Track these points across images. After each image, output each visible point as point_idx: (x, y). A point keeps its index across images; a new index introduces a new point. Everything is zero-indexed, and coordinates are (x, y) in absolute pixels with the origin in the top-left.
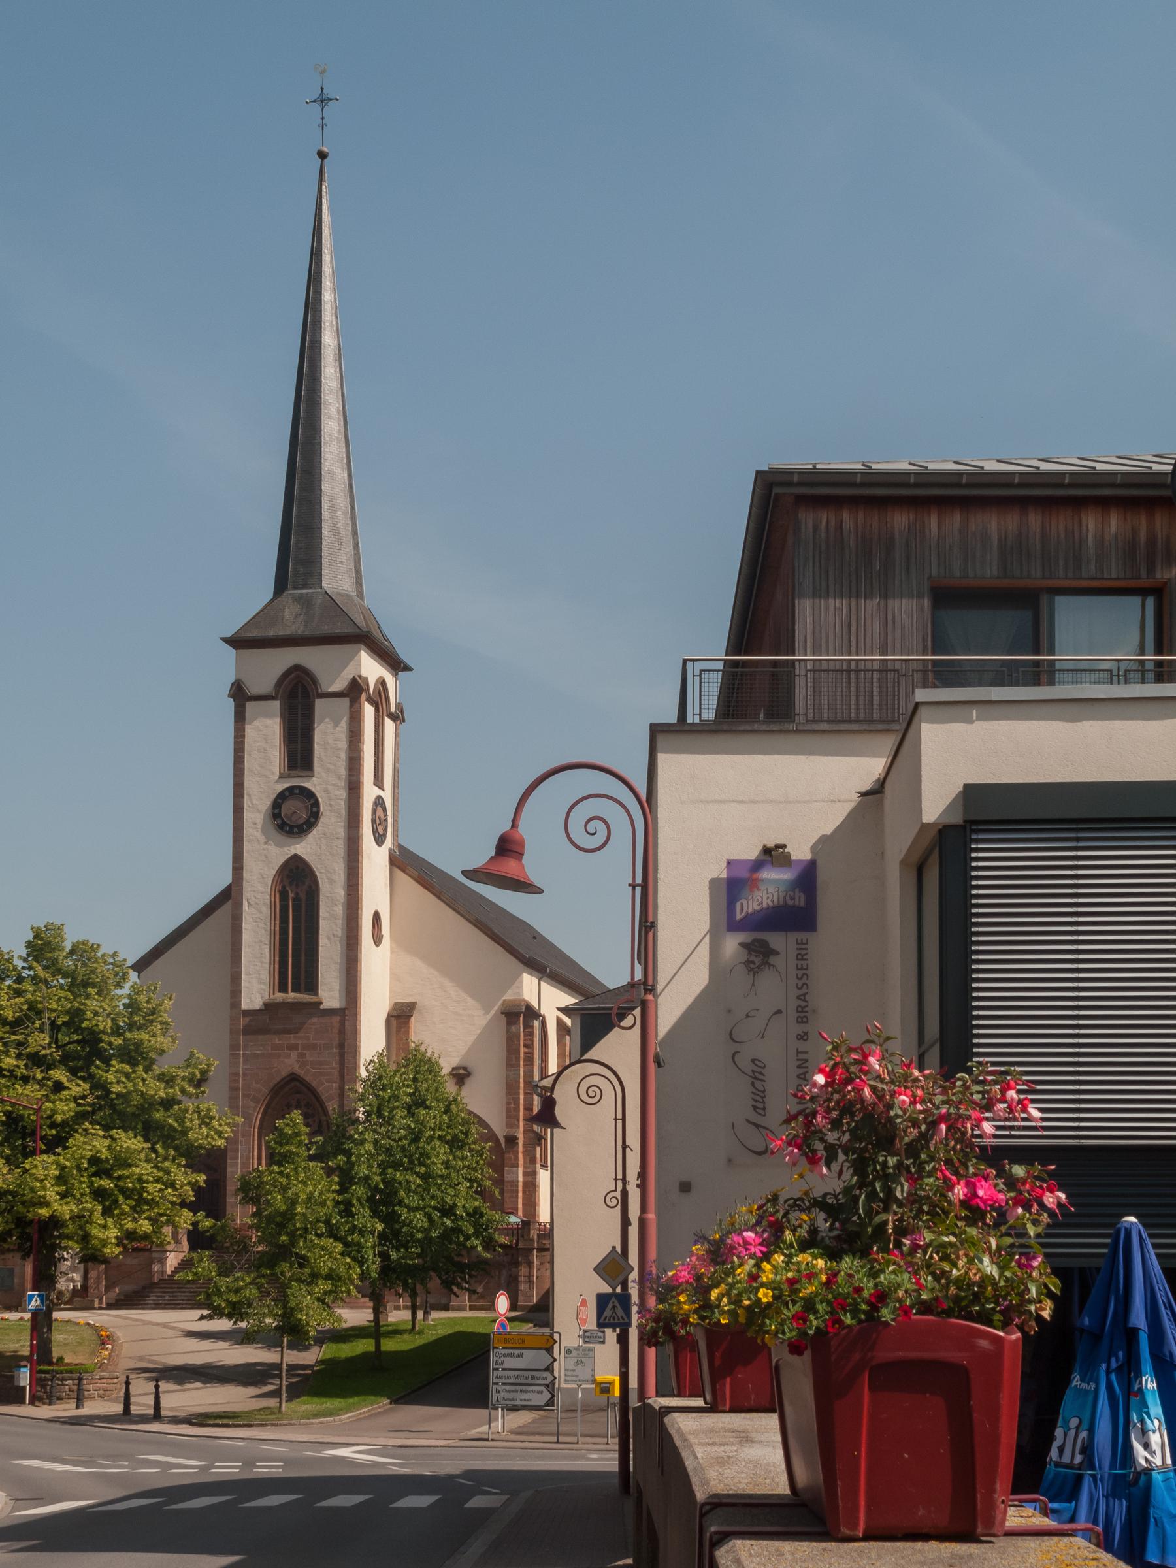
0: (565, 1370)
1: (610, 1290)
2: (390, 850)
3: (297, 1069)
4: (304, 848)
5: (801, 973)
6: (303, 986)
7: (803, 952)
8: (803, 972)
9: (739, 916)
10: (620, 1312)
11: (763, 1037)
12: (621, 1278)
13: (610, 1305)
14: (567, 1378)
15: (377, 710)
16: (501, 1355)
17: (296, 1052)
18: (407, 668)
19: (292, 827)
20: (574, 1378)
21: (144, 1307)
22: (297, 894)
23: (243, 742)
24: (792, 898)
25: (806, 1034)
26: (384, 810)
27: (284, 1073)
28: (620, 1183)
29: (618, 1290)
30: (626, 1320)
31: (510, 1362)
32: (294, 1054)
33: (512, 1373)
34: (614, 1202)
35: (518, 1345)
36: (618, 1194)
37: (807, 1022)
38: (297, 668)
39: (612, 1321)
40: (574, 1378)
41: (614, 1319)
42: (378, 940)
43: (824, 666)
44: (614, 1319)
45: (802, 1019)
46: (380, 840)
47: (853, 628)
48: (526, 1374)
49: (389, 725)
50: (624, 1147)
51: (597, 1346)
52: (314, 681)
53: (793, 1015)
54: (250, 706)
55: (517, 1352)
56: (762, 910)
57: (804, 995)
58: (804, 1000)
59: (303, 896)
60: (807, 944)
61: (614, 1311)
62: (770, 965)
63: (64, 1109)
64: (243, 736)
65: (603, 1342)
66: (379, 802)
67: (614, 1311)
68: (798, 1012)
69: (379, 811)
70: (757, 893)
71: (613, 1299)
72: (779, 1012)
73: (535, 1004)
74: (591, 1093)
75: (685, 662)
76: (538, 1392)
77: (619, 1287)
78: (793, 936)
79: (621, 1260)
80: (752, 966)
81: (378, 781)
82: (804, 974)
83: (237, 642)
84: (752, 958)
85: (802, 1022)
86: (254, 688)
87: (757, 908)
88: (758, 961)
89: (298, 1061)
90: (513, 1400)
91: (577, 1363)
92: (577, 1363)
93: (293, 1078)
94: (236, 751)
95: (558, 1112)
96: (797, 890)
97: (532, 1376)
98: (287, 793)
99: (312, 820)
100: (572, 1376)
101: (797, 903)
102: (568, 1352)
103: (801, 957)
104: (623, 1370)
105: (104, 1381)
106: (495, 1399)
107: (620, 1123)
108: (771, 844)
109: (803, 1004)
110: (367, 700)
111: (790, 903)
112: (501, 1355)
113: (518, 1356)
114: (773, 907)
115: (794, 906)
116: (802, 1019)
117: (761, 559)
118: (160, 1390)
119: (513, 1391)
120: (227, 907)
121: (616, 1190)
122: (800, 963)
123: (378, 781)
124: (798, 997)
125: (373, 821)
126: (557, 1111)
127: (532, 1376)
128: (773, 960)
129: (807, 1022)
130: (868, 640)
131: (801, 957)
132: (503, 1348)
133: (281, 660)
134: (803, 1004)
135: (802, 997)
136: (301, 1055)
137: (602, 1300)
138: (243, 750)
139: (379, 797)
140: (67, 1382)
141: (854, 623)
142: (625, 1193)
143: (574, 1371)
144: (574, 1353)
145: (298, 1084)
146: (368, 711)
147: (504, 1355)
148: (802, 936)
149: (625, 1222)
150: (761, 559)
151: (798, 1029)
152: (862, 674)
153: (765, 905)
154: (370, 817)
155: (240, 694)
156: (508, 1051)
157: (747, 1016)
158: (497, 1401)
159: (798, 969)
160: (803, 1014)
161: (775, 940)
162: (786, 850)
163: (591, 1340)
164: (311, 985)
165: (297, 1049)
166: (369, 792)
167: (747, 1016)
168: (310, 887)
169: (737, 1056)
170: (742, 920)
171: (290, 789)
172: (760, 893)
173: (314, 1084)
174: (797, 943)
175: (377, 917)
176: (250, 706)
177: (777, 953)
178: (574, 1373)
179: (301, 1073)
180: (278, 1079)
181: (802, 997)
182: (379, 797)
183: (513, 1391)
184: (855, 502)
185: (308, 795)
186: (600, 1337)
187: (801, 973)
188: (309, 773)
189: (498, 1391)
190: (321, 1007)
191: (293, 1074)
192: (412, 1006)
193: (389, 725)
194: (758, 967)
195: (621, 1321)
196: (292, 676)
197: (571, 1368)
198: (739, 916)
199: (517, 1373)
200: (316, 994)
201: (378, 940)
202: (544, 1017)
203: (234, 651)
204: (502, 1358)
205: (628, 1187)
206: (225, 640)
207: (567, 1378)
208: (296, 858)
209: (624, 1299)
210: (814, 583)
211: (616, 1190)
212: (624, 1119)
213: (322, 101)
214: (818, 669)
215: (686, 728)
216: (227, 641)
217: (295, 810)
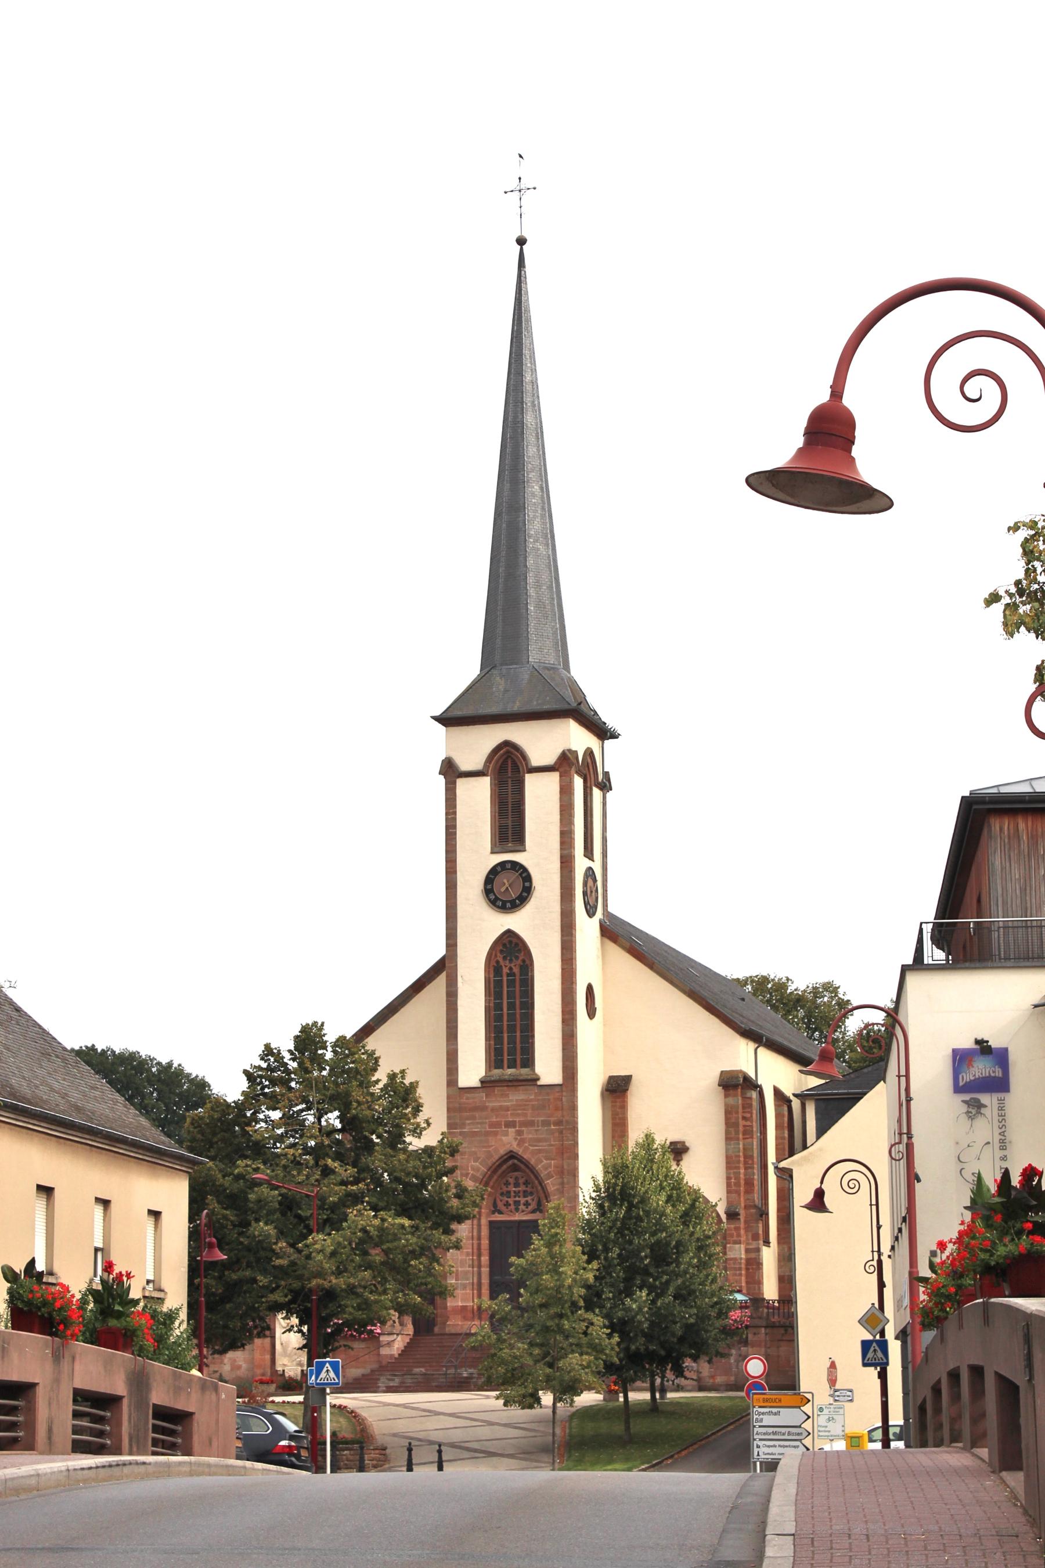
0: (818, 1426)
1: (871, 1338)
2: (600, 920)
3: (515, 1147)
4: (517, 922)
5: (1001, 1118)
6: (518, 1062)
7: (1002, 1105)
8: (1002, 1117)
9: (961, 1084)
10: (880, 1354)
11: (979, 1159)
12: (879, 1328)
13: (872, 1349)
14: (821, 1434)
15: (585, 782)
16: (760, 1414)
17: (513, 1130)
18: (614, 736)
19: (504, 903)
20: (827, 1434)
21: (375, 1390)
22: (511, 969)
23: (455, 819)
24: (994, 1072)
25: (1006, 1156)
26: (595, 880)
27: (502, 1151)
28: (876, 1255)
29: (878, 1337)
30: (885, 1361)
31: (768, 1420)
32: (511, 1130)
33: (770, 1430)
34: (872, 1269)
35: (775, 1404)
36: (875, 1263)
37: (1006, 1149)
38: (507, 744)
39: (873, 1361)
40: (827, 1434)
41: (875, 1360)
42: (591, 1013)
43: (1010, 924)
44: (875, 1360)
45: (1003, 1148)
46: (591, 912)
47: (1028, 891)
48: (783, 1430)
49: (597, 793)
50: (879, 1227)
51: (847, 1405)
52: (524, 757)
53: (997, 1145)
54: (462, 784)
55: (774, 1410)
56: (975, 1079)
57: (1003, 1132)
58: (1004, 1136)
59: (516, 970)
60: (1004, 1100)
61: (875, 1354)
62: (981, 1114)
63: (334, 1193)
64: (455, 813)
65: (851, 1401)
66: (590, 873)
67: (875, 1354)
68: (1000, 1143)
69: (590, 882)
70: (972, 1069)
71: (874, 1344)
72: (988, 1143)
73: (752, 1074)
74: (852, 1186)
75: (921, 924)
76: (795, 1447)
77: (878, 1335)
78: (995, 1096)
79: (878, 1314)
80: (970, 1115)
81: (589, 853)
82: (1003, 1119)
83: (447, 720)
84: (970, 1110)
85: (1003, 1149)
86: (465, 764)
87: (972, 1078)
88: (974, 1111)
89: (516, 1139)
90: (772, 1454)
91: (829, 1420)
92: (829, 1420)
93: (511, 1156)
94: (447, 827)
95: (827, 1200)
96: (997, 1067)
97: (789, 1432)
98: (499, 869)
99: (525, 894)
100: (825, 1431)
101: (997, 1075)
102: (821, 1410)
103: (1001, 1109)
104: (884, 1399)
105: (377, 1452)
106: (756, 1453)
107: (874, 1208)
108: (979, 1038)
109: (1003, 1138)
110: (577, 773)
111: (993, 1075)
112: (760, 1414)
113: (775, 1414)
114: (982, 1078)
115: (995, 1077)
116: (1003, 1148)
117: (969, 823)
118: (552, 1410)
119: (772, 1446)
120: (442, 980)
121: (873, 1260)
122: (1000, 1112)
123: (589, 853)
124: (1000, 1134)
125: (585, 894)
126: (826, 1199)
127: (789, 1432)
128: (983, 1110)
129: (1006, 1149)
130: (1038, 893)
131: (1001, 1109)
132: (760, 1407)
133: (489, 738)
134: (1003, 1138)
135: (1002, 1134)
136: (519, 1133)
137: (866, 1345)
138: (455, 827)
139: (590, 869)
140: (346, 1452)
141: (1028, 888)
142: (880, 1263)
143: (826, 1427)
144: (826, 1411)
145: (516, 1161)
146: (578, 782)
147: (763, 1414)
148: (1001, 1095)
149: (881, 1285)
150: (969, 823)
151: (999, 1154)
152: (1030, 930)
153: (977, 1076)
154: (582, 890)
155: (450, 771)
156: (727, 1124)
157: (969, 1146)
158: (758, 1455)
159: (999, 1116)
160: (1003, 1145)
161: (985, 1098)
162: (989, 1044)
163: (841, 1398)
164: (528, 1060)
165: (514, 1127)
166: (581, 864)
167: (969, 1146)
168: (524, 961)
169: (963, 1171)
170: (963, 1086)
171: (502, 865)
172: (974, 1069)
173: (533, 1162)
174: (998, 1100)
175: (590, 989)
176: (462, 784)
177: (985, 1106)
178: (827, 1429)
179: (520, 1151)
180: (497, 1157)
181: (1002, 1134)
182: (590, 869)
183: (772, 1446)
184: (1025, 812)
185: (517, 867)
186: (849, 1396)
187: (1001, 1118)
188: (521, 848)
189: (758, 1447)
190: (539, 1083)
191: (511, 1151)
192: (627, 1080)
193: (597, 793)
194: (974, 1115)
195: (881, 1361)
196: (502, 752)
197: (823, 1425)
198: (961, 1084)
199: (775, 1429)
200: (533, 1069)
201: (591, 1013)
202: (760, 1087)
203: (444, 728)
204: (761, 1416)
205: (882, 1258)
206: (435, 718)
207: (821, 1434)
208: (509, 932)
209: (883, 1345)
210: (1001, 863)
211: (873, 1260)
212: (877, 1205)
213: (520, 191)
214: (1006, 926)
215: (924, 967)
216: (439, 719)
217: (506, 883)
